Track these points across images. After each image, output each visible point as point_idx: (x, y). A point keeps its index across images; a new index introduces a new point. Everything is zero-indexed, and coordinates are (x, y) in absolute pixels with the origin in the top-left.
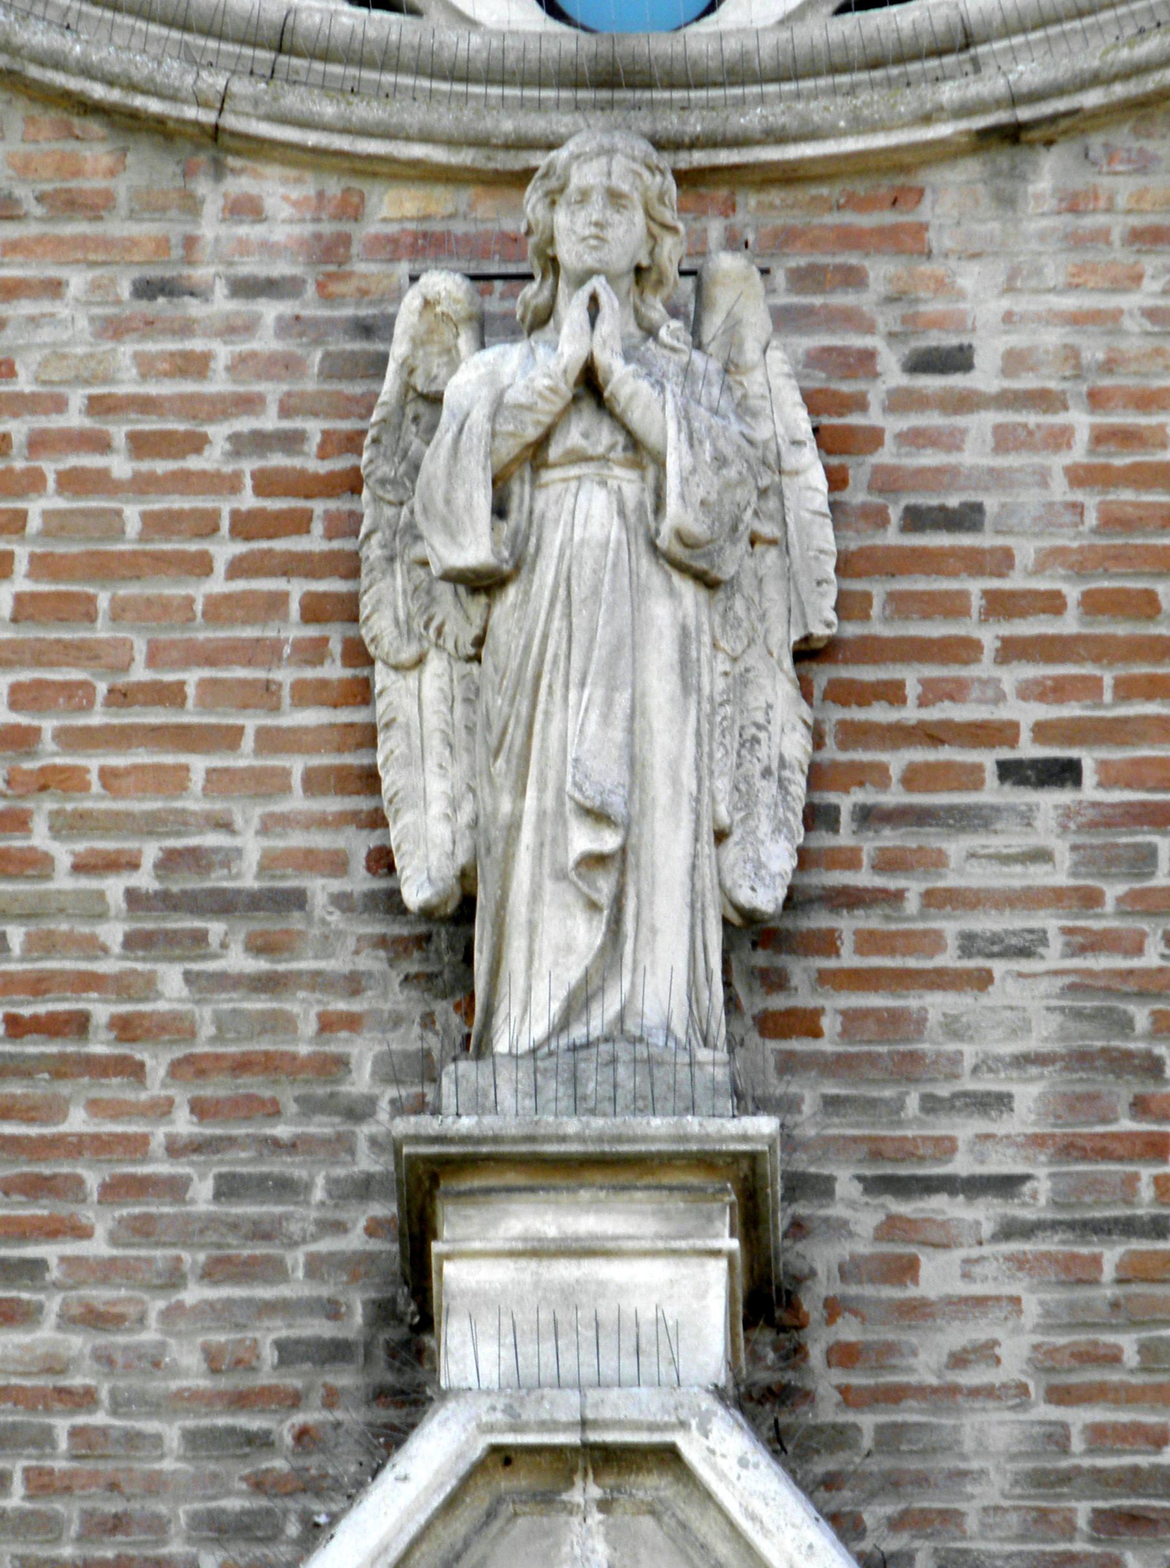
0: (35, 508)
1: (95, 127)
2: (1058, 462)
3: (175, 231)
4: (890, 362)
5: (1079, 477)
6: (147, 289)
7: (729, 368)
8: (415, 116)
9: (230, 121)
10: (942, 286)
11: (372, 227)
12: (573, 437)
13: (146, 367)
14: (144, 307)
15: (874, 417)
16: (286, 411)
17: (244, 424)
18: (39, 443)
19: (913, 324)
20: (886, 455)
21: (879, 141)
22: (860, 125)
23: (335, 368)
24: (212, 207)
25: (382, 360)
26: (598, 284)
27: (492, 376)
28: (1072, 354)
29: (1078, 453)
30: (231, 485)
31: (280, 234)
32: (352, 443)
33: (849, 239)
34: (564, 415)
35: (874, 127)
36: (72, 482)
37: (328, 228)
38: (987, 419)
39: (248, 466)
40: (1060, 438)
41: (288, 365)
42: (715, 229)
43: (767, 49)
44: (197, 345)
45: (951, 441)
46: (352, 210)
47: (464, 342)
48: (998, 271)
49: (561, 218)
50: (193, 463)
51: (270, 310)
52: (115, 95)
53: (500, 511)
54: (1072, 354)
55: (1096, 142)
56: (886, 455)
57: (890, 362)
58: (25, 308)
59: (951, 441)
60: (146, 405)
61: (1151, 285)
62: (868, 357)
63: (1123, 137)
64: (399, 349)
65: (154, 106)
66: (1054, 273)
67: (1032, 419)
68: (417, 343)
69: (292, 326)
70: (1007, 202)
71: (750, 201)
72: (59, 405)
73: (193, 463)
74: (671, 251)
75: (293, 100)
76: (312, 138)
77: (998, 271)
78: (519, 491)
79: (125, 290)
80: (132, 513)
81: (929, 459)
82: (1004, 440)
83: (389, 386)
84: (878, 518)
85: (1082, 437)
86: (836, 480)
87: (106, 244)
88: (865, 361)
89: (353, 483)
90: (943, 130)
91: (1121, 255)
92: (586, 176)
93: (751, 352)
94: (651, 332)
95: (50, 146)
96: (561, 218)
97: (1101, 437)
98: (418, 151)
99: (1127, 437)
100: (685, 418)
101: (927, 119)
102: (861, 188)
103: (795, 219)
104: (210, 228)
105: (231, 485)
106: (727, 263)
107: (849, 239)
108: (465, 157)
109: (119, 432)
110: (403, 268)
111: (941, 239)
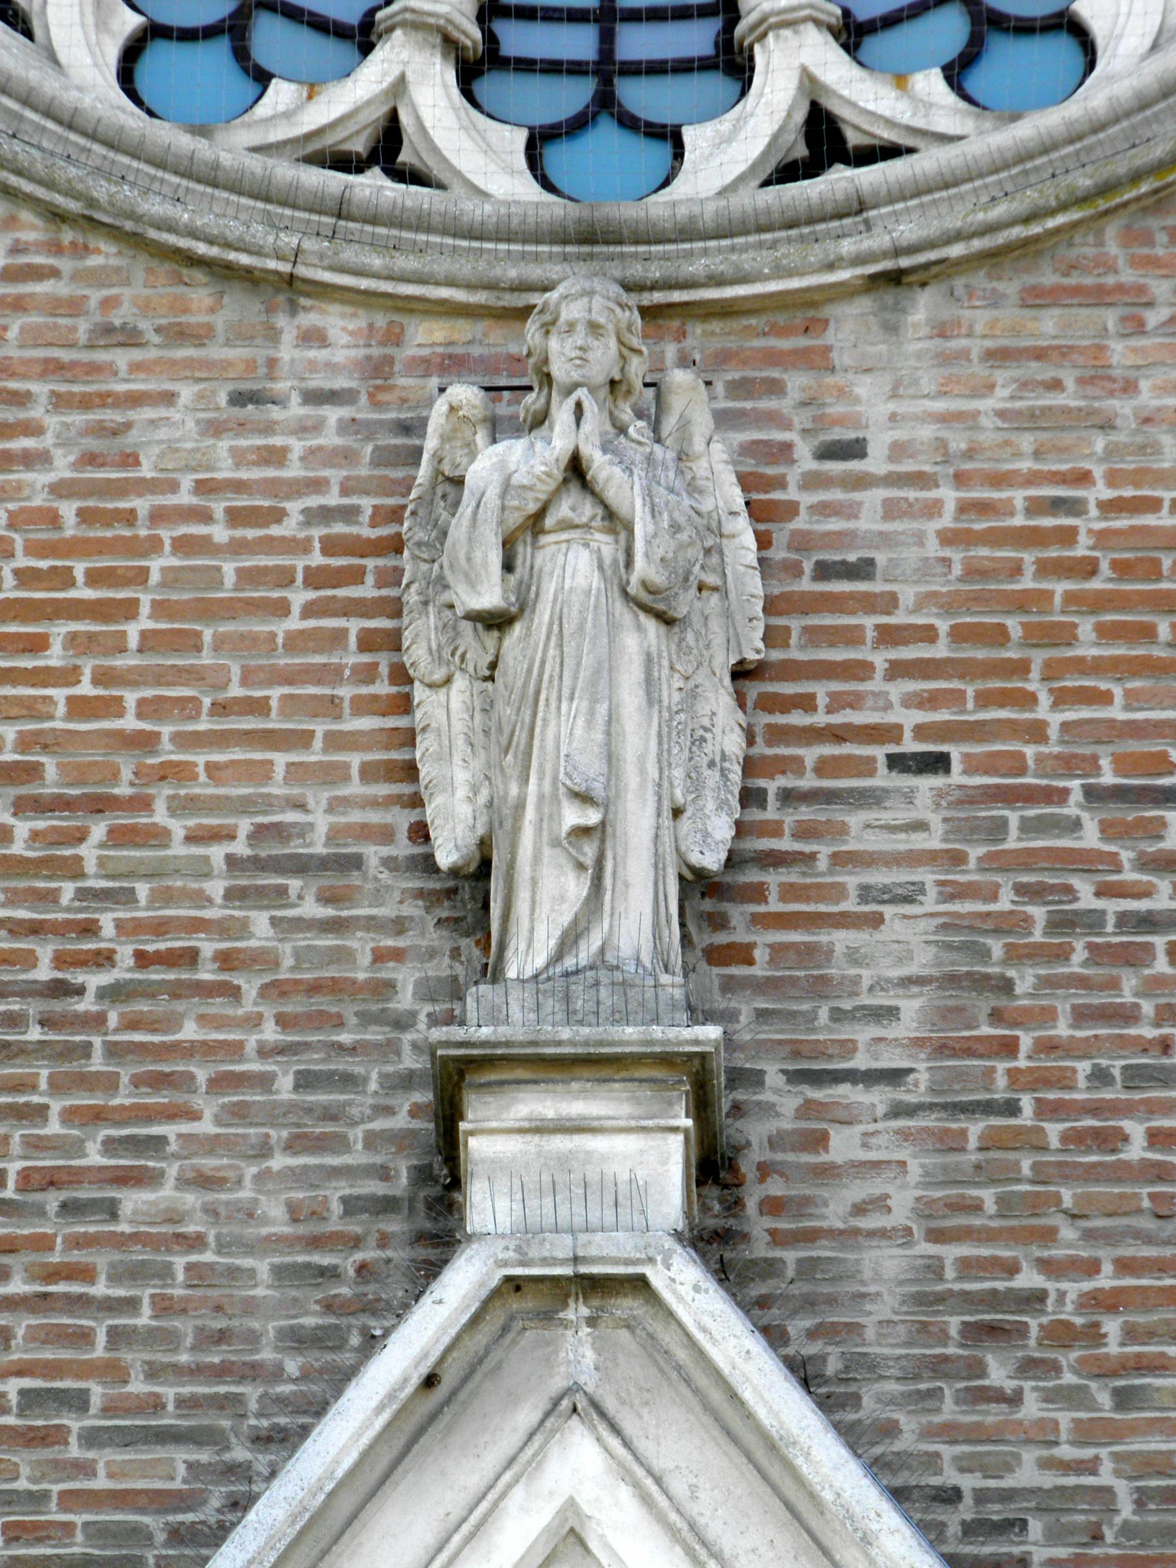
0: (156, 565)
1: (199, 275)
3: (261, 354)
4: (804, 451)
5: (948, 538)
6: (239, 399)
8: (442, 266)
9: (302, 271)
10: (843, 393)
11: (410, 351)
12: (564, 509)
13: (239, 457)
14: (237, 412)
15: (791, 493)
16: (345, 491)
17: (313, 501)
18: (158, 516)
19: (821, 422)
20: (800, 523)
21: (795, 283)
22: (780, 272)
23: (383, 458)
24: (288, 336)
25: (418, 452)
26: (582, 393)
27: (502, 464)
28: (941, 445)
29: (947, 520)
30: (303, 547)
31: (340, 356)
32: (395, 515)
33: (773, 358)
34: (556, 493)
35: (790, 273)
36: (183, 545)
37: (376, 352)
38: (880, 493)
39: (317, 532)
40: (933, 509)
41: (347, 456)
42: (671, 351)
44: (278, 441)
45: (850, 511)
46: (395, 337)
47: (481, 438)
48: (884, 382)
49: (554, 344)
50: (275, 531)
51: (333, 414)
52: (214, 252)
54: (941, 445)
55: (959, 283)
56: (800, 523)
57: (804, 451)
58: (147, 413)
59: (850, 511)
60: (239, 487)
61: (1001, 392)
62: (787, 447)
63: (980, 280)
64: (431, 444)
65: (244, 259)
66: (927, 383)
67: (912, 494)
68: (445, 439)
69: (350, 426)
70: (892, 329)
71: (697, 330)
73: (275, 531)
74: (637, 369)
75: (349, 254)
76: (364, 284)
77: (884, 382)
78: (523, 552)
79: (222, 399)
80: (229, 569)
81: (834, 525)
82: (891, 510)
83: (424, 472)
84: (795, 570)
85: (950, 508)
86: (763, 541)
87: (206, 364)
89: (396, 545)
92: (572, 311)
93: (698, 445)
94: (622, 430)
95: (165, 291)
96: (554, 344)
97: (964, 508)
98: (444, 293)
99: (984, 508)
100: (649, 494)
101: (831, 267)
102: (781, 319)
103: (731, 343)
104: (286, 352)
105: (303, 547)
106: (680, 377)
107: (773, 358)
108: (480, 297)
109: (218, 508)
110: (434, 382)
111: (841, 358)
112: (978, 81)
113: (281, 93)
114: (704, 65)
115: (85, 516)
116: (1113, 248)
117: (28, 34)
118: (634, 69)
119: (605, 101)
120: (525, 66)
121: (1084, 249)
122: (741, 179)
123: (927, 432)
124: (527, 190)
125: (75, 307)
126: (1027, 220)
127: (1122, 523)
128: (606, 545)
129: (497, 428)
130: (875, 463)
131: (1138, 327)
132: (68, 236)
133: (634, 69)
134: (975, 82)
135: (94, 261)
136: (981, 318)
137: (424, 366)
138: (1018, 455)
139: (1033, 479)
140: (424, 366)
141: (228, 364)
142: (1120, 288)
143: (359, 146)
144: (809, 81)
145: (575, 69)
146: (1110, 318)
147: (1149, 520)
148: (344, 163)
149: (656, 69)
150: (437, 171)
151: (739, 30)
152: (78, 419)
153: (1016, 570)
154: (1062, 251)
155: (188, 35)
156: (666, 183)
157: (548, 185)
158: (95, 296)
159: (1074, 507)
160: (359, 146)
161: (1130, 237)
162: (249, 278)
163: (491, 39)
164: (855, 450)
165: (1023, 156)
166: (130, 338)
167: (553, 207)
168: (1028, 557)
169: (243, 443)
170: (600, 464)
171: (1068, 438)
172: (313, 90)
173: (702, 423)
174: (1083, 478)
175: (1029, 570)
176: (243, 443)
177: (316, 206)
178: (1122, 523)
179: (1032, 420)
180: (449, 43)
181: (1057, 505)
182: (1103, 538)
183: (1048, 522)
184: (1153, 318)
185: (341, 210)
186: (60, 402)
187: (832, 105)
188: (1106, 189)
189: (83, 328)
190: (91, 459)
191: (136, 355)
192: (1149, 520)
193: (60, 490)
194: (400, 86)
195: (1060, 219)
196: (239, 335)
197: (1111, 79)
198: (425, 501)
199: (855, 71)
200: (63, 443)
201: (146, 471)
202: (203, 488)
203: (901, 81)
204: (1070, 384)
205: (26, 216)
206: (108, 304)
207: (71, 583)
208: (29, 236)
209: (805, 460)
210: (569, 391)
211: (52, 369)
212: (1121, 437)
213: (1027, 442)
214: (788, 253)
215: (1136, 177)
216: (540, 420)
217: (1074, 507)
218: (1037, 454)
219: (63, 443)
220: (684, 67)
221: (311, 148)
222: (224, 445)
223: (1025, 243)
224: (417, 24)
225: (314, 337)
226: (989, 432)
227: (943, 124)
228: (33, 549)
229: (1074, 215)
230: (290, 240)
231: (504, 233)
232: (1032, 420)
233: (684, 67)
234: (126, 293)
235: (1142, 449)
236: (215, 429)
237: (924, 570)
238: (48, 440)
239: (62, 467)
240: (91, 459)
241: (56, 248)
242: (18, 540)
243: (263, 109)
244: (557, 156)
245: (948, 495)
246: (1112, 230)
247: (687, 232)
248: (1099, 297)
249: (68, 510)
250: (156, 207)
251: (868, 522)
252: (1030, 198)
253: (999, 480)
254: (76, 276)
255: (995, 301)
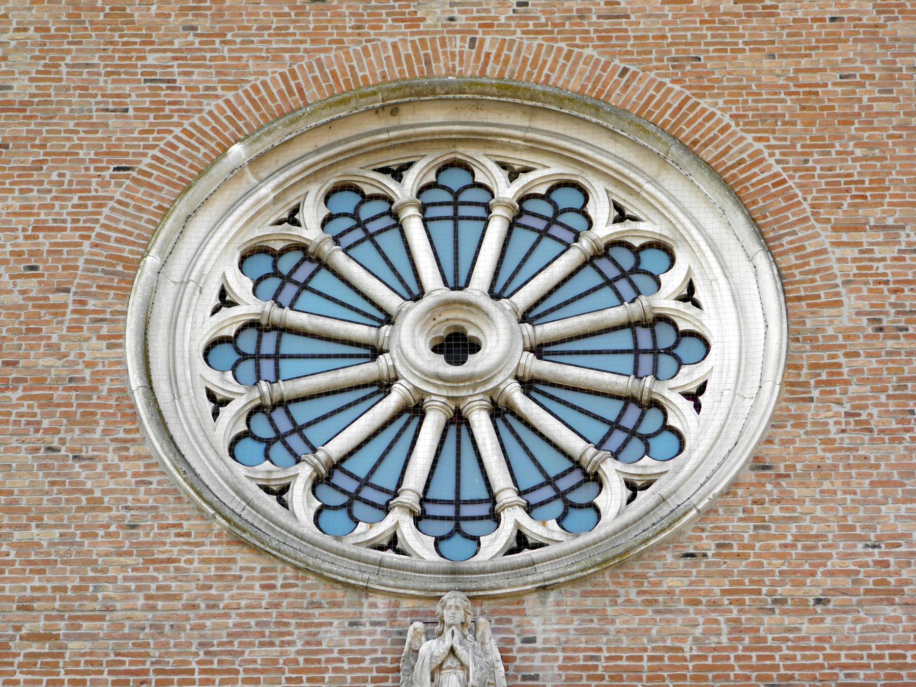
0: (327, 676)
1: (339, 586)
2: (556, 664)
3: (358, 610)
4: (518, 641)
5: (561, 668)
6: (352, 624)
7: (483, 644)
8: (411, 584)
9: (370, 585)
10: (529, 623)
11: (401, 610)
12: (448, 663)
13: (352, 642)
14: (351, 628)
15: (514, 654)
16: (383, 653)
17: (374, 656)
18: (328, 661)
19: (523, 632)
20: (517, 663)
21: (515, 590)
22: (510, 586)
23: (394, 642)
24: (366, 605)
25: (405, 641)
26: (453, 628)
27: (430, 648)
28: (558, 639)
29: (560, 663)
30: (371, 670)
31: (381, 611)
32: (398, 660)
33: (508, 612)
34: (447, 658)
35: (513, 587)
36: (335, 670)
37: (392, 610)
38: (540, 654)
39: (375, 666)
40: (556, 659)
41: (383, 642)
42: (478, 610)
43: (489, 565)
44: (363, 637)
45: (531, 659)
46: (397, 605)
47: (423, 638)
48: (541, 619)
49: (445, 612)
50: (362, 665)
51: (379, 629)
52: (344, 579)
53: (432, 680)
54: (558, 639)
55: (563, 589)
56: (517, 663)
57: (518, 641)
58: (324, 629)
59: (531, 659)
60: (351, 651)
61: (576, 623)
62: (513, 639)
63: (569, 588)
64: (408, 639)
65: (353, 582)
66: (554, 620)
67: (550, 654)
68: (413, 638)
69: (384, 633)
70: (543, 603)
71: (486, 603)
72: (332, 652)
73: (362, 665)
74: (469, 618)
75: (384, 581)
76: (388, 589)
77: (541, 619)
78: (436, 676)
79: (346, 624)
80: (349, 677)
81: (527, 664)
82: (544, 659)
83: (406, 647)
84: (516, 678)
85: (561, 659)
86: (506, 669)
87: (342, 613)
88: (512, 641)
89: (398, 670)
90: (529, 587)
91: (568, 616)
92: (451, 602)
93: (487, 640)
94: (465, 637)
95: (329, 591)
96: (445, 612)
97: (565, 659)
98: (412, 592)
99: (571, 659)
100: (474, 659)
101: (525, 585)
102: (511, 600)
103: (496, 607)
104: (365, 610)
105: (371, 670)
106: (482, 620)
107: (508, 612)
108: (422, 593)
109: (345, 658)
110: (409, 619)
111: (528, 612)
112: (566, 523)
113: (362, 527)
114: (487, 517)
115: (306, 661)
116: (608, 579)
117: (287, 508)
118: (466, 519)
119: (457, 529)
120: (435, 518)
121: (600, 579)
122: (498, 553)
123: (554, 635)
124: (436, 557)
125: (303, 596)
126: (582, 571)
127: (612, 664)
128: (461, 673)
129: (429, 635)
130: (539, 644)
131: (615, 603)
132: (300, 574)
133: (466, 519)
134: (565, 523)
135: (308, 582)
136: (569, 600)
137: (406, 614)
138: (581, 642)
139: (585, 650)
140: (406, 614)
141: (348, 613)
142: (610, 591)
143: (385, 543)
144: (517, 524)
145: (449, 519)
146: (607, 600)
147: (619, 663)
148: (381, 548)
149: (473, 518)
150: (408, 551)
151: (497, 507)
152: (304, 630)
153: (581, 678)
154: (593, 580)
155: (336, 508)
156: (476, 553)
157: (442, 556)
158: (309, 592)
159: (597, 659)
160: (385, 543)
161: (613, 576)
162: (354, 587)
163: (424, 511)
164: (532, 640)
165: (580, 549)
166: (319, 606)
167: (444, 563)
168: (584, 674)
169: (353, 638)
170: (459, 649)
171: (595, 637)
172: (371, 524)
173: (488, 633)
174: (600, 650)
175: (585, 678)
176: (353, 638)
177: (374, 563)
178: (612, 664)
179: (584, 631)
180: (412, 512)
181: (593, 658)
182: (606, 668)
183: (590, 663)
184: (620, 600)
185: (381, 564)
186: (299, 625)
187: (524, 531)
188: (605, 561)
189: (305, 602)
190: (308, 643)
191: (321, 611)
192: (619, 663)
193: (299, 653)
194: (397, 525)
195: (592, 570)
196: (351, 605)
197: (606, 525)
198: (407, 657)
199: (532, 521)
200: (300, 638)
201: (324, 647)
202: (341, 652)
203: (544, 524)
204: (596, 620)
205: (288, 568)
206: (312, 595)
207: (302, 682)
208: (289, 574)
209: (518, 644)
210: (450, 626)
211: (296, 615)
212: (611, 637)
213: (583, 638)
214: (513, 581)
215: (614, 558)
216: (441, 633)
217: (597, 659)
218: (586, 642)
219: (300, 638)
220: (481, 518)
221: (370, 544)
222: (347, 638)
223: (582, 577)
224: (402, 506)
225: (373, 605)
226: (572, 635)
227: (557, 536)
228: (291, 671)
229: (596, 569)
230: (366, 576)
231: (428, 571)
232: (584, 631)
233: (481, 518)
234: (318, 592)
235: (617, 641)
236: (344, 634)
237: (554, 678)
238: (295, 637)
239: (299, 646)
240: (308, 643)
241: (297, 578)
242: (286, 668)
243: (357, 531)
244: (443, 545)
245: (561, 655)
246: (607, 574)
247: (482, 571)
248: (604, 594)
249: (301, 659)
250: (326, 566)
251: (537, 663)
252: (583, 564)
253: (575, 650)
254: (304, 587)
255: (573, 595)
